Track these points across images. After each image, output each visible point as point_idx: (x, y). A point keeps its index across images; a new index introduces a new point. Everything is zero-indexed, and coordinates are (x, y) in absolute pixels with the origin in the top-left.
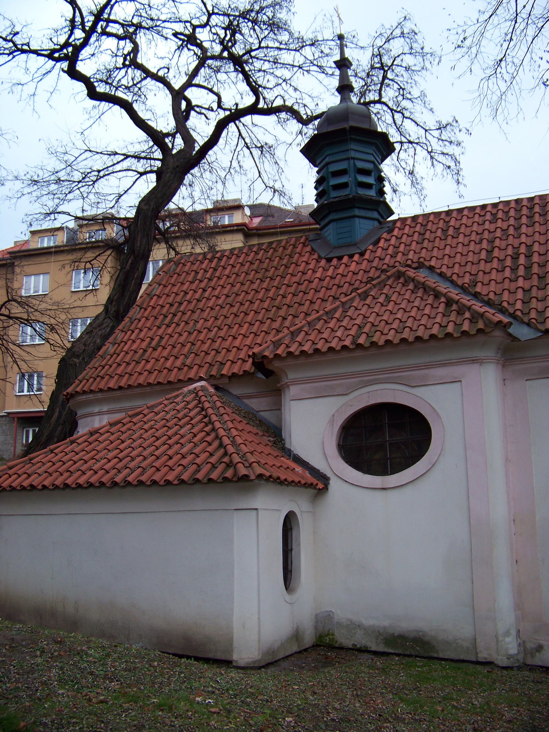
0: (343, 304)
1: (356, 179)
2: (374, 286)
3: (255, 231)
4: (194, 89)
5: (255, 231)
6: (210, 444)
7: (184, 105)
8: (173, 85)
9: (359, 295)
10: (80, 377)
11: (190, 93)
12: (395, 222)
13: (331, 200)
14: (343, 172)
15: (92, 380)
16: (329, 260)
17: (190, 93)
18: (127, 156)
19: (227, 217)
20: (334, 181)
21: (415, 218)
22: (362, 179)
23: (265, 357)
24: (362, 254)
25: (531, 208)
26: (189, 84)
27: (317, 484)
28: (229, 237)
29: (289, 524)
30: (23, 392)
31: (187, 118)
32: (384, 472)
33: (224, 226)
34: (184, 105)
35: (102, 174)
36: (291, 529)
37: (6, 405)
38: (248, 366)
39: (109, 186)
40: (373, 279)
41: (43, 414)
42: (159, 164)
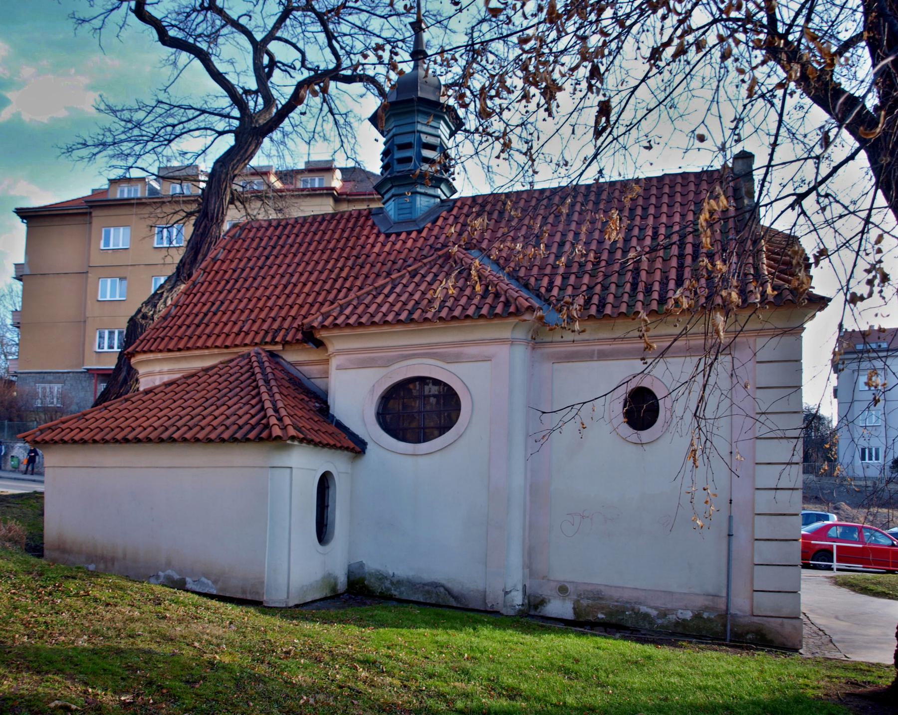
0: (393, 280)
1: (420, 153)
2: (425, 264)
3: (345, 197)
4: (276, 42)
5: (345, 197)
6: (253, 407)
7: (266, 60)
8: (255, 36)
9: (409, 272)
10: (141, 338)
11: (273, 46)
12: (456, 201)
13: (396, 174)
14: (408, 146)
15: (152, 340)
16: (388, 236)
17: (273, 46)
18: (203, 112)
19: (317, 179)
20: (399, 155)
21: (474, 198)
22: (427, 153)
23: (313, 327)
24: (420, 232)
25: (586, 196)
26: (271, 36)
27: (356, 447)
28: (318, 201)
29: (325, 483)
30: (113, 348)
31: (270, 75)
32: (418, 441)
33: (314, 189)
34: (266, 60)
35: (178, 129)
36: (328, 487)
37: (86, 360)
38: (299, 336)
39: (191, 143)
40: (426, 257)
41: (111, 372)
42: (236, 123)
